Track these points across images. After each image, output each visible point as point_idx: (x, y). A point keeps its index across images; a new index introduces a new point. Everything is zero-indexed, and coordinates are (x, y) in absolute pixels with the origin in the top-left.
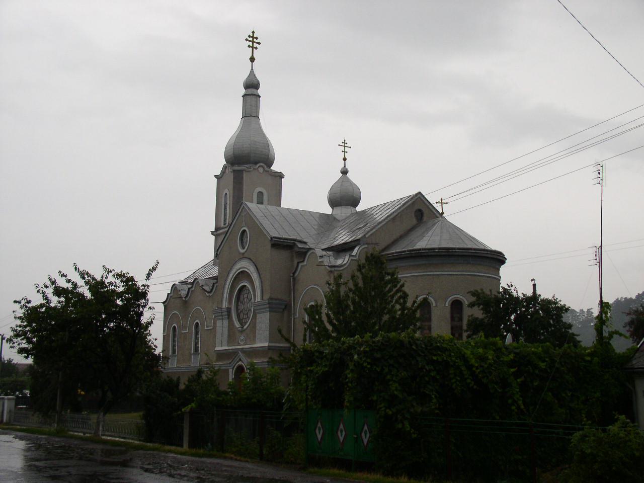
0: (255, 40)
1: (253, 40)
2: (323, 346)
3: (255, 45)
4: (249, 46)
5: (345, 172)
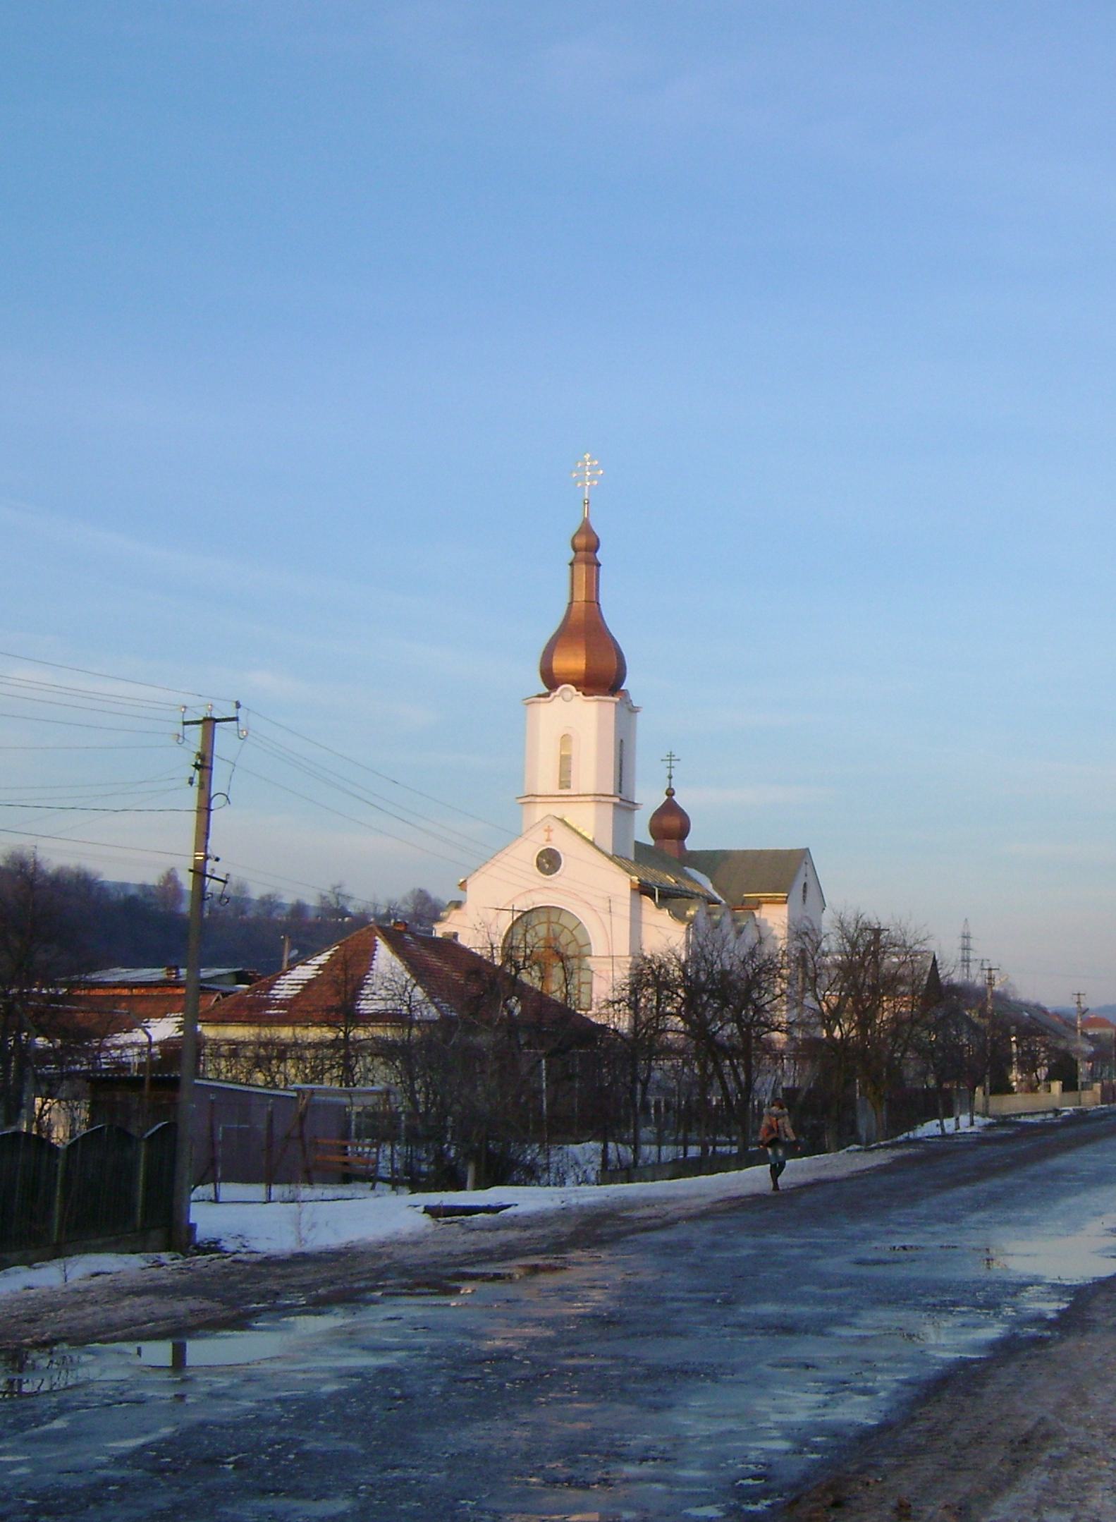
5: (670, 793)
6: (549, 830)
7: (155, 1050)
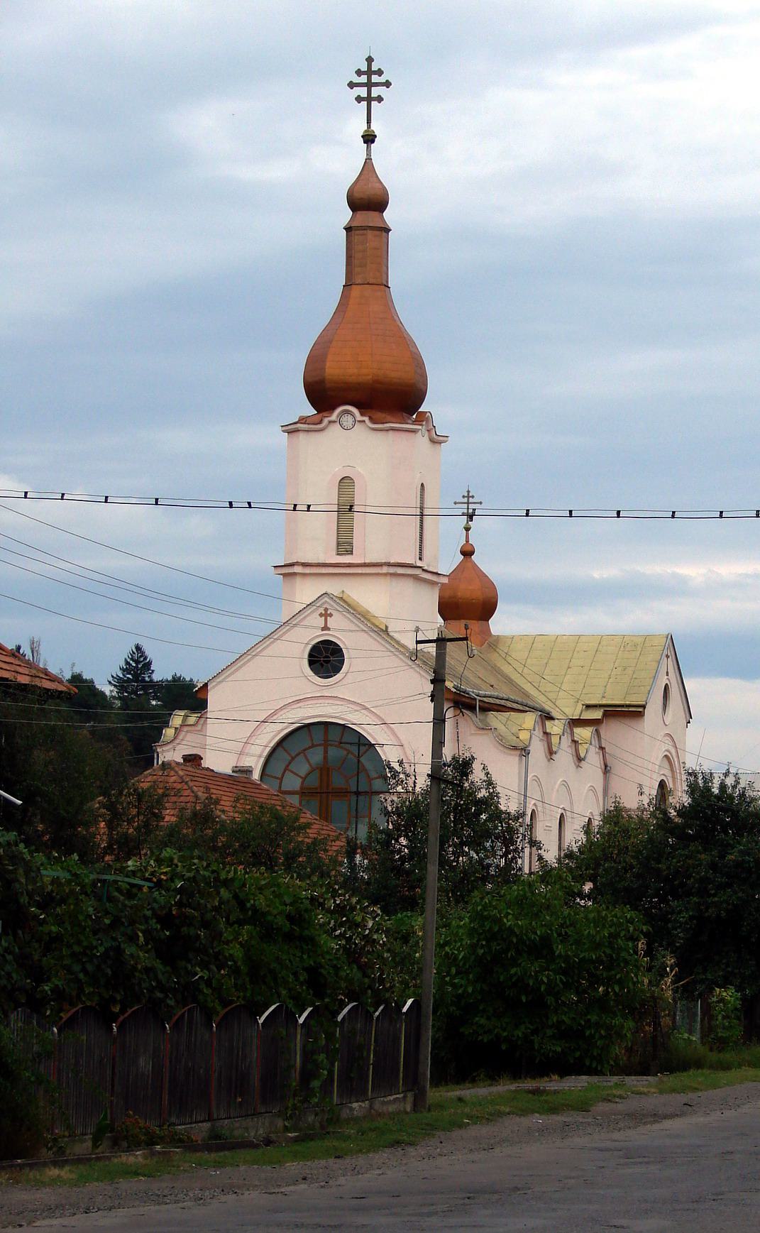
0: (375, 79)
1: (369, 79)
2: (602, 1004)
3: (375, 92)
4: (359, 99)
5: (467, 553)
6: (326, 615)
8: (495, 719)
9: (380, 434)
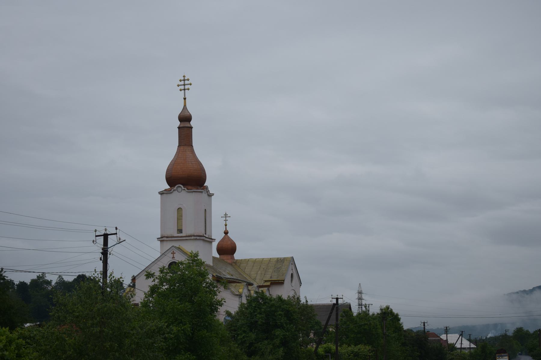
3: (187, 87)
5: (226, 233)
6: (173, 253)
7: (472, 350)
8: (232, 287)
9: (191, 193)
